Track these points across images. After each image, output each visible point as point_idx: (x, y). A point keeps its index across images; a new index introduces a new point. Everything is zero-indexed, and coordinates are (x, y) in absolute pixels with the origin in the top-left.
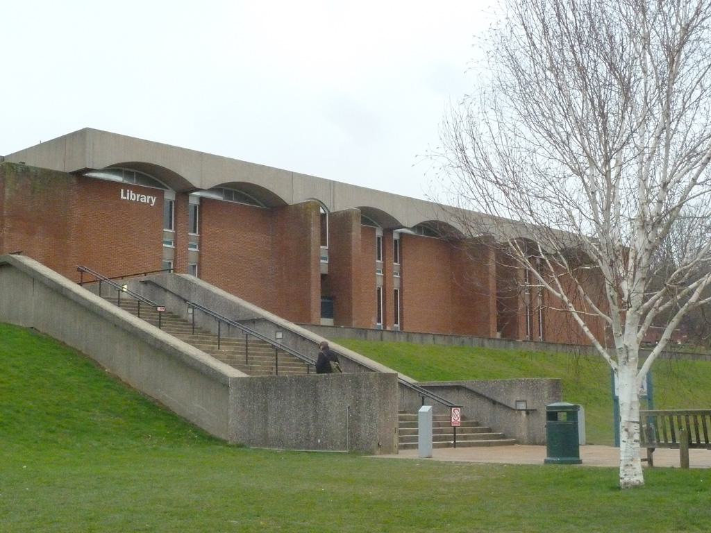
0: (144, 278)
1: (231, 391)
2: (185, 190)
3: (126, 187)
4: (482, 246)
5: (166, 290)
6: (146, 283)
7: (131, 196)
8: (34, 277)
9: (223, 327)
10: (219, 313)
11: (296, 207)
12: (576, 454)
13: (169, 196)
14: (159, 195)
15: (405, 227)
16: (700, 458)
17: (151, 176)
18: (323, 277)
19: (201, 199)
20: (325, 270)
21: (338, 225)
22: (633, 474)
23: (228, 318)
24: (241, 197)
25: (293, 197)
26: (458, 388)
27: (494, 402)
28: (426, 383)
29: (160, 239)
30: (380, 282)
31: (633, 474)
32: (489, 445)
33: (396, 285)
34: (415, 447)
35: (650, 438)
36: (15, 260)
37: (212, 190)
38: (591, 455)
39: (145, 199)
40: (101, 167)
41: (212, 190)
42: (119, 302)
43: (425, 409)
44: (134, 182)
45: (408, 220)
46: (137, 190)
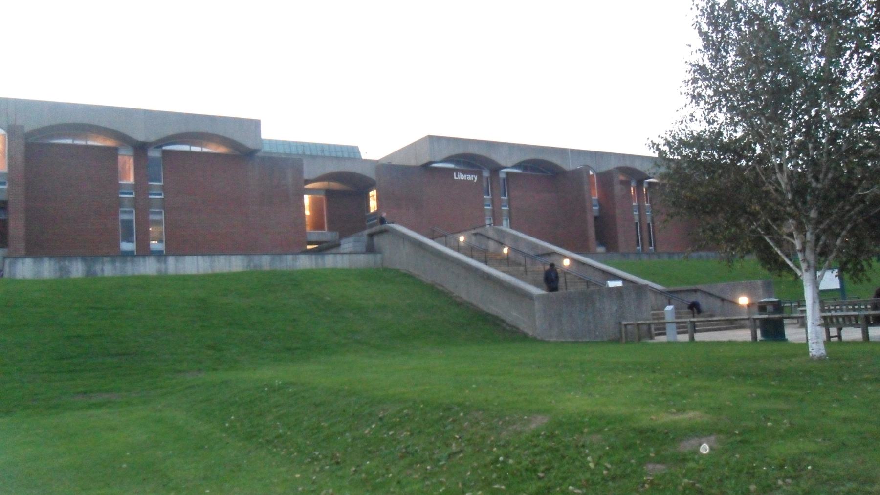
0: (473, 232)
1: (536, 303)
2: (495, 169)
3: (457, 171)
4: (577, 177)
5: (489, 238)
6: (475, 234)
7: (461, 177)
8: (404, 237)
9: (527, 259)
10: (525, 250)
11: (574, 172)
12: (782, 335)
13: (486, 174)
14: (480, 175)
15: (506, 167)
16: (877, 332)
17: (185, 148)
18: (596, 218)
19: (508, 174)
20: (596, 214)
21: (606, 179)
22: (816, 349)
23: (532, 253)
24: (533, 169)
25: (569, 166)
26: (696, 291)
27: (723, 300)
28: (671, 288)
29: (483, 203)
30: (636, 219)
31: (816, 349)
32: (720, 330)
33: (649, 220)
34: (664, 334)
35: (827, 322)
36: (391, 228)
37: (515, 167)
38: (792, 333)
39: (470, 178)
40: (509, 165)
41: (515, 167)
42: (458, 249)
43: (669, 308)
44: (462, 168)
45: (508, 164)
46: (464, 172)
